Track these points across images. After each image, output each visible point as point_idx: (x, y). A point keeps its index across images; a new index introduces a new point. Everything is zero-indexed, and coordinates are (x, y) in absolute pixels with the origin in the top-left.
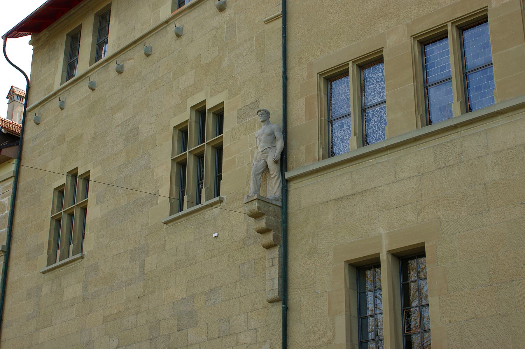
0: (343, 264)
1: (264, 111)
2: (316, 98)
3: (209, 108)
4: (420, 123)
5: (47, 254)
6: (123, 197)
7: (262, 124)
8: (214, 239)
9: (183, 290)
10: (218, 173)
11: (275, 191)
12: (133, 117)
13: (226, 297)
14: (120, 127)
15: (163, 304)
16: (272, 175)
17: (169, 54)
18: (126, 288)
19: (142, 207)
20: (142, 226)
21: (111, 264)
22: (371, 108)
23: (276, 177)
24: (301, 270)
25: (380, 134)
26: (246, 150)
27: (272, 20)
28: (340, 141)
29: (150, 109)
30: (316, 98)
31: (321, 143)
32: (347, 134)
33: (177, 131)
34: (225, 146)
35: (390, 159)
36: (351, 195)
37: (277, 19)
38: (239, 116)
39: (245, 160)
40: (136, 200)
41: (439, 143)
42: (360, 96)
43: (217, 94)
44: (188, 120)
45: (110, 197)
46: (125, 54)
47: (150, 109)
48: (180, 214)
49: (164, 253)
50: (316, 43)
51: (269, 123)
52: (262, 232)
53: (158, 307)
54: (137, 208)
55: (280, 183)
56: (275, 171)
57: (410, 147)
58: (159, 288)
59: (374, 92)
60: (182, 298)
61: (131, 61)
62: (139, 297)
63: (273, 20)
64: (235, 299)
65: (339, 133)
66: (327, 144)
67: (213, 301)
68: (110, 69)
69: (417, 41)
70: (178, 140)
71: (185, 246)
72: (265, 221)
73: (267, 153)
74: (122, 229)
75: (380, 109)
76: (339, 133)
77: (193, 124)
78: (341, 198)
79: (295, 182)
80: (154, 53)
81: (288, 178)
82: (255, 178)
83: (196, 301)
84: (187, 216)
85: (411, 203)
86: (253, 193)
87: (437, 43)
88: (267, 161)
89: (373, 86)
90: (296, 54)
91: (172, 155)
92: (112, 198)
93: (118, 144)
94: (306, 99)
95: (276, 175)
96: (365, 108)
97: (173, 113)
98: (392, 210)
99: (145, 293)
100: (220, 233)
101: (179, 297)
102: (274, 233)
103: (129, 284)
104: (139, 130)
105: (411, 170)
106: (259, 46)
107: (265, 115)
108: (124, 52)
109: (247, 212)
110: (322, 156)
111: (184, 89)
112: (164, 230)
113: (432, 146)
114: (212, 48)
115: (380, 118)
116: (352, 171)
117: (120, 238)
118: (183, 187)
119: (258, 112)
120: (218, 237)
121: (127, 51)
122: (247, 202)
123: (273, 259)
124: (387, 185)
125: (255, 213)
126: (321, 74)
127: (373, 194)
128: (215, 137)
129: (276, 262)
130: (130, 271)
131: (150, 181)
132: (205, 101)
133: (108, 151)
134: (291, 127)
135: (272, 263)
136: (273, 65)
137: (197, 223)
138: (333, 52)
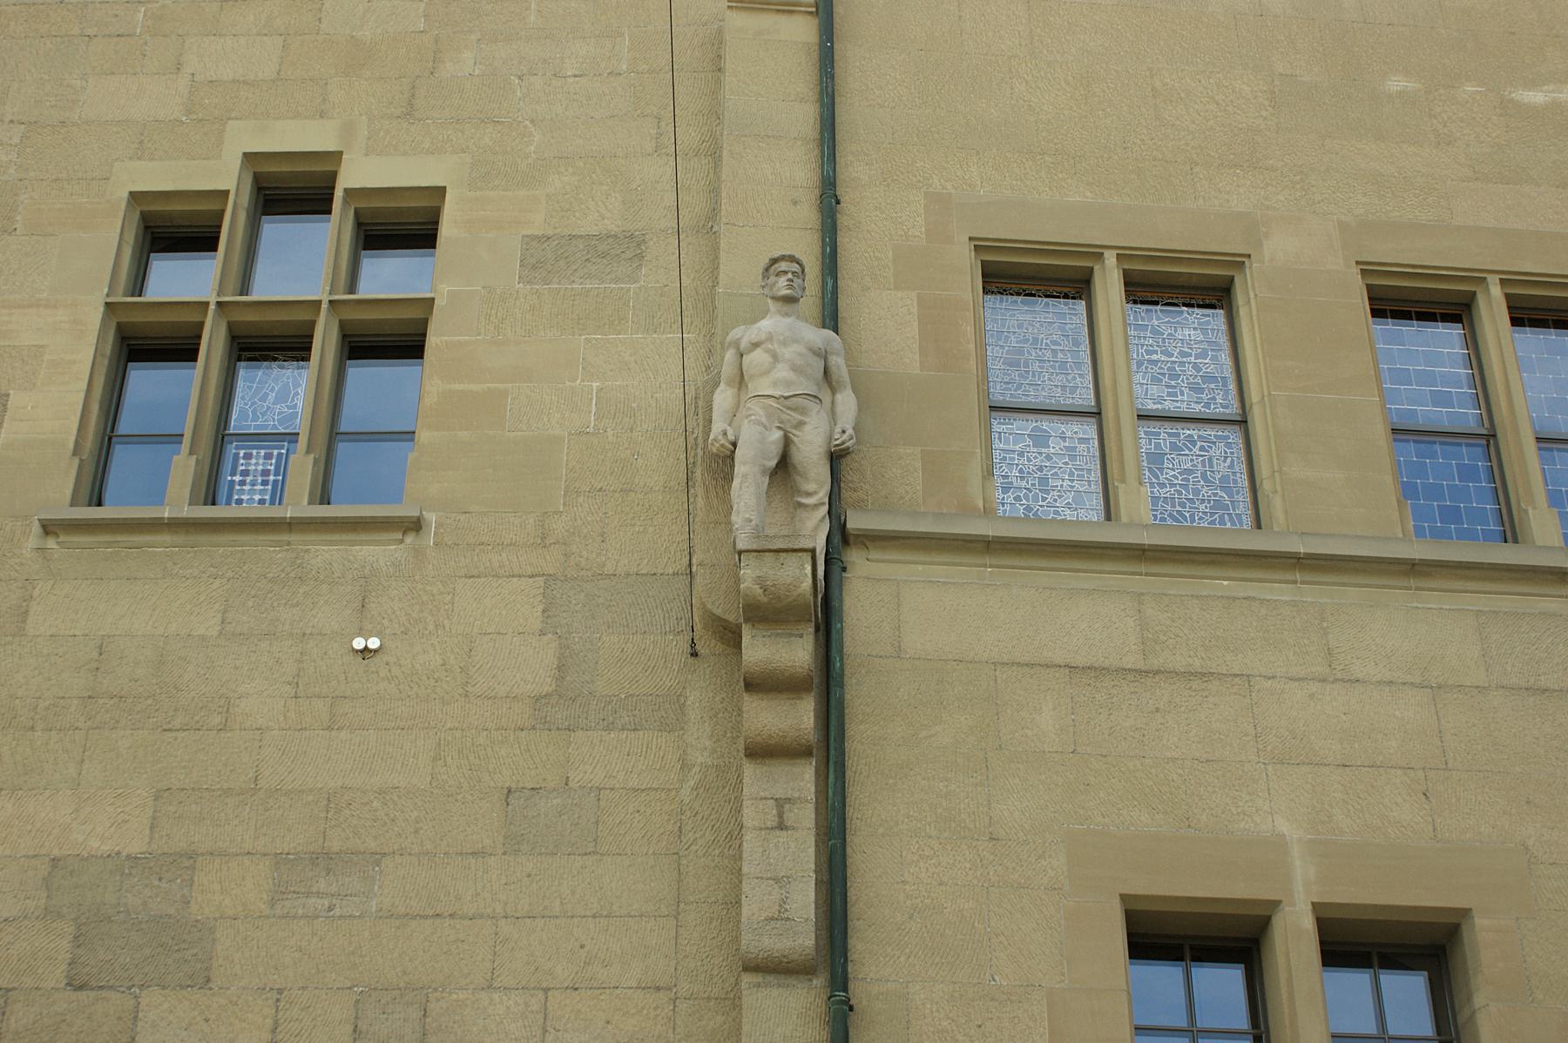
16: (809, 494)
37: (784, 11)
57: (1384, 587)
78: (1097, 671)
91: (110, 287)
94: (918, 298)
113: (1472, 611)
120: (378, 659)
123: (781, 803)
127: (1235, 694)
129: (805, 817)
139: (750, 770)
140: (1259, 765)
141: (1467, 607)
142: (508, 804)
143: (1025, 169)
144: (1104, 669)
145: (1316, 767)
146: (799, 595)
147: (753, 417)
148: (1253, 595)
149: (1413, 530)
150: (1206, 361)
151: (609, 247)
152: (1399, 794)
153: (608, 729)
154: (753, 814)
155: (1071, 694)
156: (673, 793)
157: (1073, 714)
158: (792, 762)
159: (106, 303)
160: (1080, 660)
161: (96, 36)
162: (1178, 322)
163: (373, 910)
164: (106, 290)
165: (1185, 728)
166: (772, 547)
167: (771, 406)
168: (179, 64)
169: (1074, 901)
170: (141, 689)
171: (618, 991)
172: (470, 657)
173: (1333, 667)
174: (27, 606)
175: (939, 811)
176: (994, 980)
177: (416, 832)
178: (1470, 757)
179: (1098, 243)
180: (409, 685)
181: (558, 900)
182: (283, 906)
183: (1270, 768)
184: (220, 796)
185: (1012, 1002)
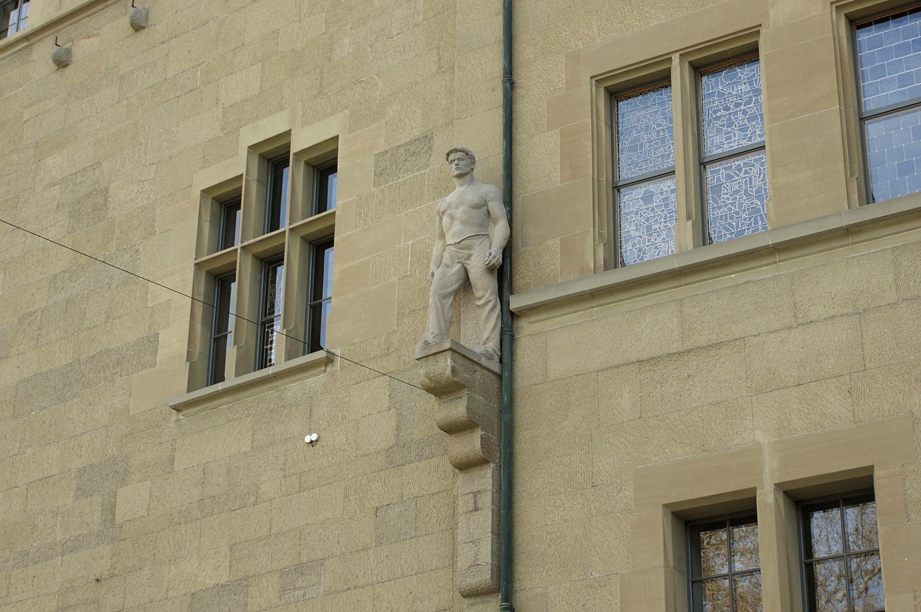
0: (660, 511)
1: (463, 152)
2: (589, 131)
3: (299, 150)
4: (855, 196)
5: (185, 359)
6: (60, 346)
7: (456, 182)
8: (306, 448)
9: (219, 566)
10: (312, 299)
11: (485, 336)
12: (94, 167)
13: (338, 584)
14: (57, 187)
15: (164, 598)
16: (480, 299)
17: (194, 27)
18: (64, 558)
19: (114, 371)
20: (110, 413)
21: (24, 502)
22: (724, 162)
23: (490, 306)
24: (548, 522)
25: (745, 219)
26: (398, 246)
28: (643, 232)
29: (140, 150)
30: (589, 131)
31: (600, 233)
32: (661, 218)
33: (210, 200)
34: (341, 236)
35: (781, 273)
36: (679, 353)
38: (380, 170)
39: (393, 269)
40: (97, 354)
41: (908, 243)
42: (696, 133)
43: (319, 120)
44: (242, 175)
45: (27, 347)
46: (75, 24)
47: (140, 150)
48: (220, 389)
49: (169, 478)
50: (587, 11)
51: (472, 181)
52: (452, 429)
53: (150, 603)
54: (99, 373)
55: (497, 319)
56: (487, 291)
57: (831, 249)
58: (155, 558)
59: (729, 125)
60: (218, 584)
61: (91, 39)
62: (98, 580)
64: (361, 590)
65: (641, 215)
66: (612, 238)
67: (302, 592)
68: (34, 56)
69: (843, 16)
70: (210, 222)
71: (228, 462)
72: (465, 404)
73: (469, 247)
74: (56, 421)
75: (744, 164)
76: (641, 215)
77: (254, 186)
78: (655, 359)
79: (533, 318)
80: (155, 25)
81: (516, 308)
82: (441, 303)
83: (255, 592)
84: (234, 393)
85: (837, 377)
86: (434, 337)
87: (891, 24)
88: (468, 267)
89: (727, 113)
90: (535, 33)
92: (30, 350)
93: (51, 226)
95: (490, 301)
96: (705, 161)
97: (202, 160)
98: (787, 391)
99: (116, 572)
100: (323, 435)
101: (208, 581)
102: (484, 432)
103: (72, 549)
104: (109, 194)
105: (835, 300)
106: (434, 16)
107: (464, 162)
108: (78, 18)
109: (423, 379)
110: (603, 263)
111: (232, 105)
112: (172, 424)
114: (309, 16)
115: (746, 185)
116: (683, 299)
117: (51, 442)
118: (218, 330)
119: (448, 155)
120: (319, 443)
121: (84, 18)
122: (424, 357)
123: (476, 494)
124: (774, 332)
126: (598, 80)
128: (309, 217)
129: (487, 500)
130: (76, 519)
131: (137, 311)
132: (288, 133)
133: (25, 241)
134: (523, 194)
135: (475, 503)
136: (476, 55)
137: (260, 411)
138: (631, 31)
140: (747, 398)
141: (886, 247)
143: (625, 13)
144: (659, 357)
145: (782, 390)
146: (447, 378)
148: (749, 280)
149: (857, 200)
150: (751, 106)
151: (416, 147)
152: (833, 396)
153: (420, 460)
154: (463, 505)
155: (640, 379)
156: (450, 492)
157: (640, 393)
158: (481, 468)
159: (195, 264)
160: (646, 355)
161: (181, 96)
162: (735, 83)
163: (322, 592)
164: (194, 256)
165: (705, 384)
166: (430, 353)
167: (452, 250)
168: (217, 99)
169: (636, 516)
170: (222, 490)
172: (358, 433)
173: (797, 316)
174: (174, 454)
175: (565, 475)
176: (592, 576)
177: (338, 543)
178: (881, 356)
179: (666, 52)
180: (332, 457)
181: (400, 568)
182: (285, 598)
183: (754, 399)
184: (256, 542)
185: (601, 587)
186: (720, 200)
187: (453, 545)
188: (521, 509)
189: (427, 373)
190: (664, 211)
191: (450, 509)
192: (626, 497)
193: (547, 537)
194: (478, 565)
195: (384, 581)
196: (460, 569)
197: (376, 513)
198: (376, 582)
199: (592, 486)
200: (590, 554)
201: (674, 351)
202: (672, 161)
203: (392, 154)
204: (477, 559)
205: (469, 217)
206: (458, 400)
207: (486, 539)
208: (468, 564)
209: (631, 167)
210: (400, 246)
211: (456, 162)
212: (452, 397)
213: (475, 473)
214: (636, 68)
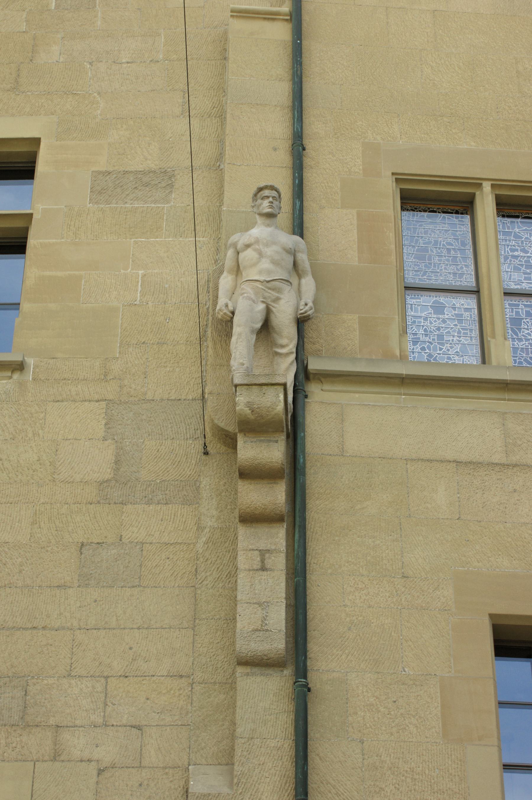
26: (122, 271)
27: (257, 16)
43: (13, 115)
56: (291, 341)
63: (258, 18)
64: (53, 632)
116: (506, 413)
123: (263, 553)
125: (269, 417)
139: (242, 531)
142: (81, 553)
147: (245, 295)
156: (192, 546)
157: (458, 493)
158: (271, 525)
160: (463, 458)
166: (257, 382)
167: (257, 287)
171: (154, 678)
172: (56, 455)
175: (369, 558)
177: (20, 572)
179: (478, 176)
181: (115, 618)
186: (520, 333)
187: (195, 605)
188: (312, 582)
189: (249, 402)
190: (457, 326)
191: (191, 565)
192: (444, 597)
193: (345, 619)
194: (267, 630)
195: (89, 628)
196: (241, 630)
197: (81, 549)
198: (78, 627)
199: (403, 576)
200: (402, 648)
201: (496, 461)
202: (465, 281)
203: (116, 177)
204: (266, 624)
205: (282, 260)
206: (271, 443)
207: (279, 604)
208: (252, 628)
209: (419, 273)
210: (126, 272)
211: (271, 199)
212: (262, 438)
213: (263, 530)
214: (441, 181)
